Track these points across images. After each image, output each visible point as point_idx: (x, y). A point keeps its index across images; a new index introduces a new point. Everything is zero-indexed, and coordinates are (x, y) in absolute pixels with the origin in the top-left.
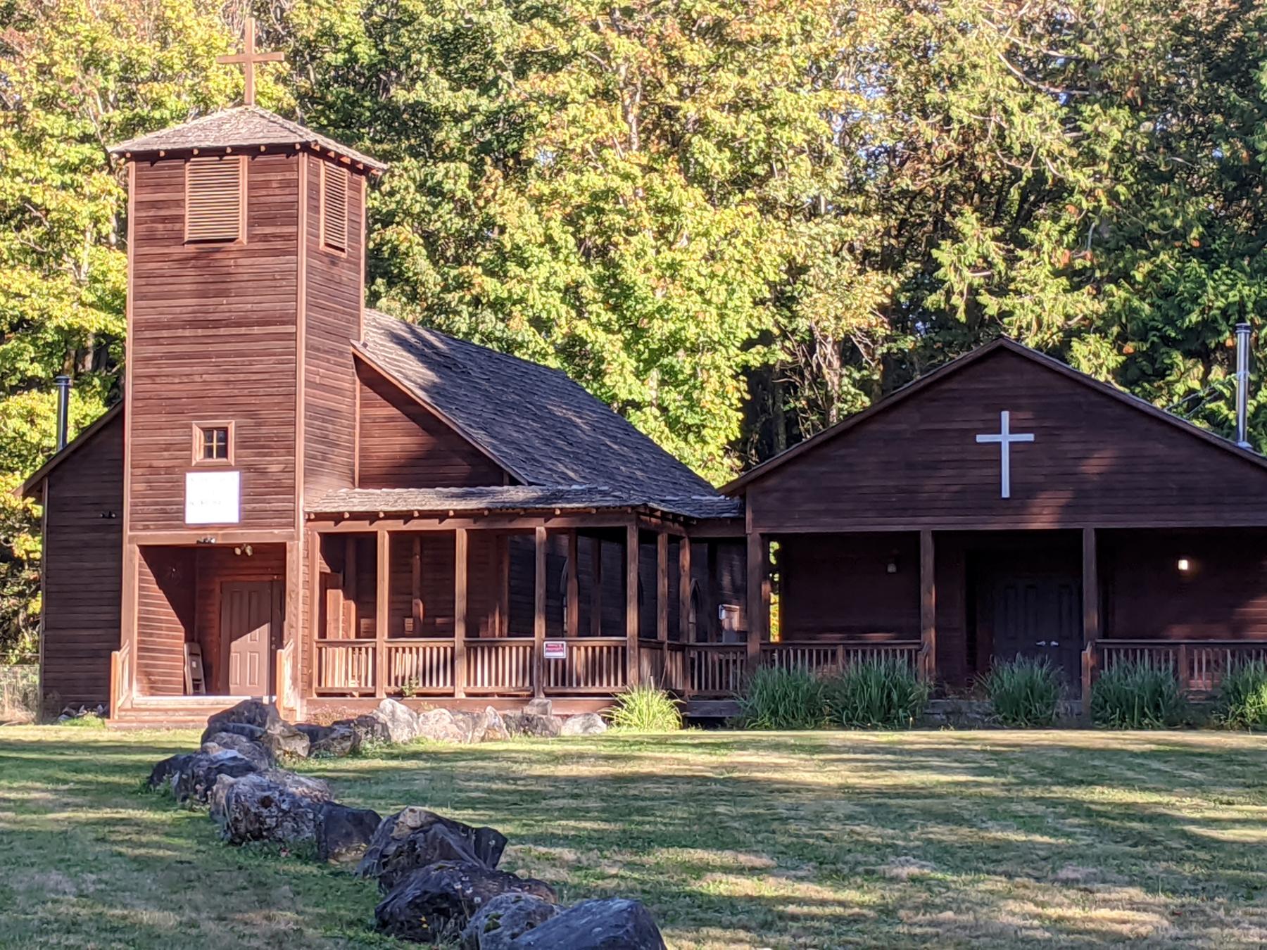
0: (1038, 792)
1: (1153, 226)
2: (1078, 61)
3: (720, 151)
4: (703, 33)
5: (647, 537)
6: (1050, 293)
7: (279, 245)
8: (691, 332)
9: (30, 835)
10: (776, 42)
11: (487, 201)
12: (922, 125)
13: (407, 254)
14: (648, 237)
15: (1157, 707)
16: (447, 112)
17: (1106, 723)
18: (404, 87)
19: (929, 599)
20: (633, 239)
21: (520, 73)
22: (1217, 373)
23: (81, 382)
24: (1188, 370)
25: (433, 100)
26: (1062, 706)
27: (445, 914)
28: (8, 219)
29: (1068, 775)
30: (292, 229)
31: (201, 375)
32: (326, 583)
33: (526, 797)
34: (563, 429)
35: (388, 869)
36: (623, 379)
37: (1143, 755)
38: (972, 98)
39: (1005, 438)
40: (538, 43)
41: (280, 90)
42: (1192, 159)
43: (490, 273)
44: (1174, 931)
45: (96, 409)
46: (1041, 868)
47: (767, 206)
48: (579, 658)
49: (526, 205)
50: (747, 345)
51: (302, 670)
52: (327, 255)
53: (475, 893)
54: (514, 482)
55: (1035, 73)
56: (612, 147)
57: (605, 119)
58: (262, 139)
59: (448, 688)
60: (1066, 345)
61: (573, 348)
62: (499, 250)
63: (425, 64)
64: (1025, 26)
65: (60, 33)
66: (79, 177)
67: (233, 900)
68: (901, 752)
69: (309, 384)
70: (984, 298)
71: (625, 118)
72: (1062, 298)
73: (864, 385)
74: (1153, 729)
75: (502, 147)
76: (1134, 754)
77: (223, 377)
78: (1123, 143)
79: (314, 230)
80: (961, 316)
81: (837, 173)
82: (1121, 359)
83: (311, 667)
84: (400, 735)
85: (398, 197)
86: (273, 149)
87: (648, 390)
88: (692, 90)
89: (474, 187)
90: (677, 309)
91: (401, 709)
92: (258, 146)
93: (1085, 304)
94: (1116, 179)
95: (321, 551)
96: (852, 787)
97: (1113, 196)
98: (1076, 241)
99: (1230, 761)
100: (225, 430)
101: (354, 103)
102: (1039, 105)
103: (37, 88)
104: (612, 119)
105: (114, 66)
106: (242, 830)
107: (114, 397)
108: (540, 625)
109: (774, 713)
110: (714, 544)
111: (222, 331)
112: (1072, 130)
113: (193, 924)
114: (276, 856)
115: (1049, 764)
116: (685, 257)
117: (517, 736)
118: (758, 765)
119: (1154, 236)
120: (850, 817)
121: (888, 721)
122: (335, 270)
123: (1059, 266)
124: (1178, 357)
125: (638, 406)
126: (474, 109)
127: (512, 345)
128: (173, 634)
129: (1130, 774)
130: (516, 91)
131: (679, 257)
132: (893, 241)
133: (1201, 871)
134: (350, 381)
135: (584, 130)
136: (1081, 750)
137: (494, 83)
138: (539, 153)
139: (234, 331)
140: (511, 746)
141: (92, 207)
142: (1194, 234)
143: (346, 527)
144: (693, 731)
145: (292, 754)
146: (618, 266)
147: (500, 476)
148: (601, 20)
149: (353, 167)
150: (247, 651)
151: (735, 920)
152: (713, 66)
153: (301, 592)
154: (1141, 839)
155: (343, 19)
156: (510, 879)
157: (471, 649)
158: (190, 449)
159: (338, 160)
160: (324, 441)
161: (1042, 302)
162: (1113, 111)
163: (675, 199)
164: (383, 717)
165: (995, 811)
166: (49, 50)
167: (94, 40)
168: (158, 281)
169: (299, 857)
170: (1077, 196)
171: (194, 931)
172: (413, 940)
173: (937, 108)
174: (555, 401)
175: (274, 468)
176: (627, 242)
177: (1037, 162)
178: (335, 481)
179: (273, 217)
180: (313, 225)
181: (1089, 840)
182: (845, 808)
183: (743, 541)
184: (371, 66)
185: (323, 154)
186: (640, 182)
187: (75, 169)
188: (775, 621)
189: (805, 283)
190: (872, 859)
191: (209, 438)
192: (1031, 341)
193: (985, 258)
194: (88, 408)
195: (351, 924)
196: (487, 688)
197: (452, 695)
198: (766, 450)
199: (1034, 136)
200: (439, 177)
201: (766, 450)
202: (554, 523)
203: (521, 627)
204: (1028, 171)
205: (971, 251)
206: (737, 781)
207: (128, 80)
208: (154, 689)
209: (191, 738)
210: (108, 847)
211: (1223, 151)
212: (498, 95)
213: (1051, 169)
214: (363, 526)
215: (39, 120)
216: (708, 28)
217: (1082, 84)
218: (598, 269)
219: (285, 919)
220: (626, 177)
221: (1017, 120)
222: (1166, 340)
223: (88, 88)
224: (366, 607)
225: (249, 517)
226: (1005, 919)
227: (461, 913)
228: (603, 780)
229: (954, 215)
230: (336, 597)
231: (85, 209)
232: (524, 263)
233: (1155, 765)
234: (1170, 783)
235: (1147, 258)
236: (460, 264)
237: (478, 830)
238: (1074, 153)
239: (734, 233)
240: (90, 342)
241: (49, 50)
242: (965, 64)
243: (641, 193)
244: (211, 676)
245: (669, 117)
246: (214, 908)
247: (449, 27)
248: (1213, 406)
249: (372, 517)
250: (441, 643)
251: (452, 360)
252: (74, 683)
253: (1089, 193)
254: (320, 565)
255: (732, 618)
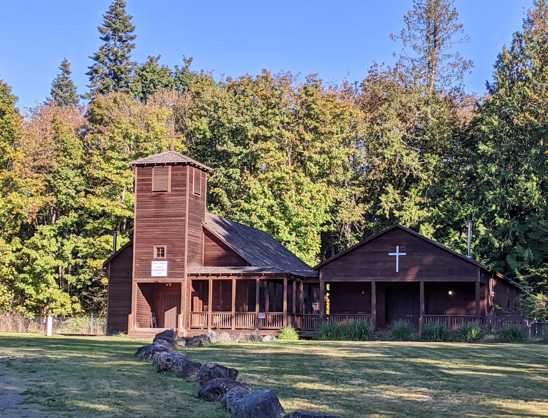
0: (401, 360)
1: (446, 190)
2: (424, 140)
3: (315, 166)
4: (311, 130)
5: (290, 283)
6: (414, 210)
7: (180, 193)
8: (305, 221)
9: (98, 369)
10: (333, 133)
11: (245, 180)
12: (376, 159)
13: (221, 196)
14: (293, 192)
15: (441, 335)
16: (234, 153)
17: (426, 340)
18: (220, 145)
19: (374, 301)
20: (289, 192)
21: (256, 142)
22: (464, 235)
23: (122, 233)
24: (455, 234)
25: (229, 150)
26: (412, 335)
27: (218, 394)
28: (101, 183)
29: (411, 355)
30: (185, 188)
31: (158, 232)
32: (193, 295)
33: (248, 359)
34: (266, 249)
35: (202, 380)
36: (284, 234)
37: (435, 349)
38: (391, 151)
39: (397, 254)
40: (261, 133)
41: (183, 146)
42: (458, 170)
43: (246, 202)
44: (433, 401)
45: (127, 240)
46: (397, 382)
47: (329, 183)
48: (270, 318)
49: (257, 182)
50: (322, 225)
51: (183, 322)
52: (195, 196)
53: (226, 387)
54: (250, 265)
55: (411, 144)
56: (283, 164)
57: (281, 156)
58: (175, 161)
59: (230, 327)
60: (418, 226)
61: (270, 225)
62: (249, 196)
63: (227, 138)
64: (408, 130)
65: (116, 127)
66: (122, 171)
67: (156, 389)
68: (363, 347)
69: (189, 235)
70: (395, 212)
71: (287, 156)
72: (418, 212)
73: (358, 238)
74: (439, 341)
75: (250, 165)
76: (432, 349)
77: (163, 232)
78: (437, 165)
79: (191, 189)
80: (388, 217)
81: (349, 175)
82: (435, 230)
83: (188, 320)
84: (213, 341)
85: (218, 179)
86: (179, 164)
87: (293, 238)
88: (307, 147)
89: (241, 176)
90: (301, 214)
91: (214, 333)
92: (174, 163)
93: (425, 213)
94: (435, 176)
95: (192, 285)
96: (347, 357)
97: (433, 181)
98: (422, 195)
99: (460, 351)
100: (164, 248)
101: (206, 150)
102: (412, 154)
103: (110, 144)
104: (283, 156)
105: (133, 137)
106: (161, 368)
107: (131, 237)
108: (257, 307)
109: (327, 335)
110: (310, 284)
111: (163, 219)
112: (421, 161)
113: (143, 396)
114: (171, 376)
115: (406, 352)
116: (304, 198)
117: (249, 341)
118: (320, 351)
119: (445, 193)
120: (344, 367)
121: (361, 338)
122: (197, 201)
123: (417, 202)
124: (452, 230)
125: (289, 242)
126: (241, 152)
127: (252, 224)
128: (147, 310)
129: (429, 355)
130: (254, 147)
131: (302, 198)
132: (367, 195)
133: (445, 383)
134: (201, 234)
135: (276, 160)
136: (416, 347)
137: (248, 144)
138: (261, 165)
139: (167, 219)
140: (247, 344)
141: (126, 180)
142: (458, 193)
143: (199, 278)
144: (302, 341)
145: (180, 346)
146: (284, 200)
147: (246, 263)
148: (280, 126)
149: (203, 170)
150: (170, 315)
151: (305, 396)
152: (313, 140)
153: (186, 297)
154: (429, 374)
155: (202, 125)
156: (238, 384)
157: (236, 315)
158: (153, 254)
159: (198, 167)
160: (193, 253)
161: (412, 213)
162: (434, 156)
163: (302, 180)
164: (208, 335)
165: (387, 365)
166: (113, 133)
167: (127, 129)
168: (144, 203)
169: (178, 376)
170: (423, 181)
171: (143, 398)
172: (208, 401)
173: (381, 154)
174: (262, 240)
175: (178, 260)
176: (286, 193)
177: (411, 171)
178: (196, 264)
179: (179, 184)
180: (191, 187)
181: (413, 374)
182: (342, 364)
183: (319, 284)
184: (210, 139)
185: (194, 166)
186: (291, 175)
187: (121, 168)
188: (328, 307)
189: (340, 207)
190: (348, 379)
191: (159, 251)
192: (408, 225)
193: (395, 200)
194: (122, 240)
195: (190, 396)
196: (241, 327)
197: (231, 329)
198: (328, 255)
199: (410, 163)
200: (231, 173)
201: (328, 255)
202: (262, 278)
203: (252, 309)
204: (408, 173)
205: (391, 197)
206: (313, 355)
207: (137, 142)
208: (141, 326)
209: (151, 341)
210: (121, 372)
211: (468, 168)
212: (249, 148)
213: (415, 173)
214: (205, 278)
215: (110, 153)
216: (312, 129)
217: (425, 147)
218: (278, 200)
219: (171, 394)
220: (287, 173)
221: (404, 158)
222: (448, 225)
223: (125, 144)
224: (205, 302)
225: (170, 275)
226: (384, 396)
227: (222, 393)
228: (272, 354)
229: (386, 186)
230: (196, 299)
231: (123, 181)
232: (256, 199)
233: (437, 352)
234: (441, 357)
235: (443, 200)
236: (237, 199)
237: (230, 369)
238: (421, 168)
239: (320, 191)
240: (125, 221)
241: (113, 133)
242: (390, 141)
243: (291, 178)
244: (158, 322)
245: (301, 156)
246: (150, 391)
247: (234, 127)
248: (462, 245)
249: (207, 275)
250: (228, 313)
251: (234, 229)
252: (117, 324)
253: (425, 180)
254: (192, 289)
255: (316, 307)
